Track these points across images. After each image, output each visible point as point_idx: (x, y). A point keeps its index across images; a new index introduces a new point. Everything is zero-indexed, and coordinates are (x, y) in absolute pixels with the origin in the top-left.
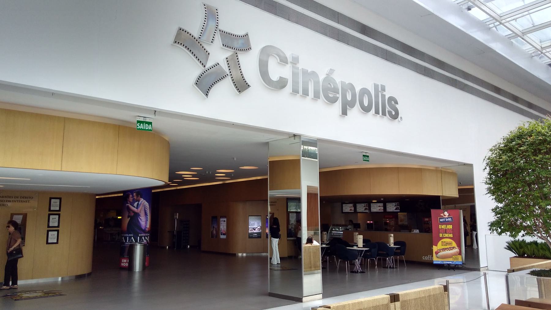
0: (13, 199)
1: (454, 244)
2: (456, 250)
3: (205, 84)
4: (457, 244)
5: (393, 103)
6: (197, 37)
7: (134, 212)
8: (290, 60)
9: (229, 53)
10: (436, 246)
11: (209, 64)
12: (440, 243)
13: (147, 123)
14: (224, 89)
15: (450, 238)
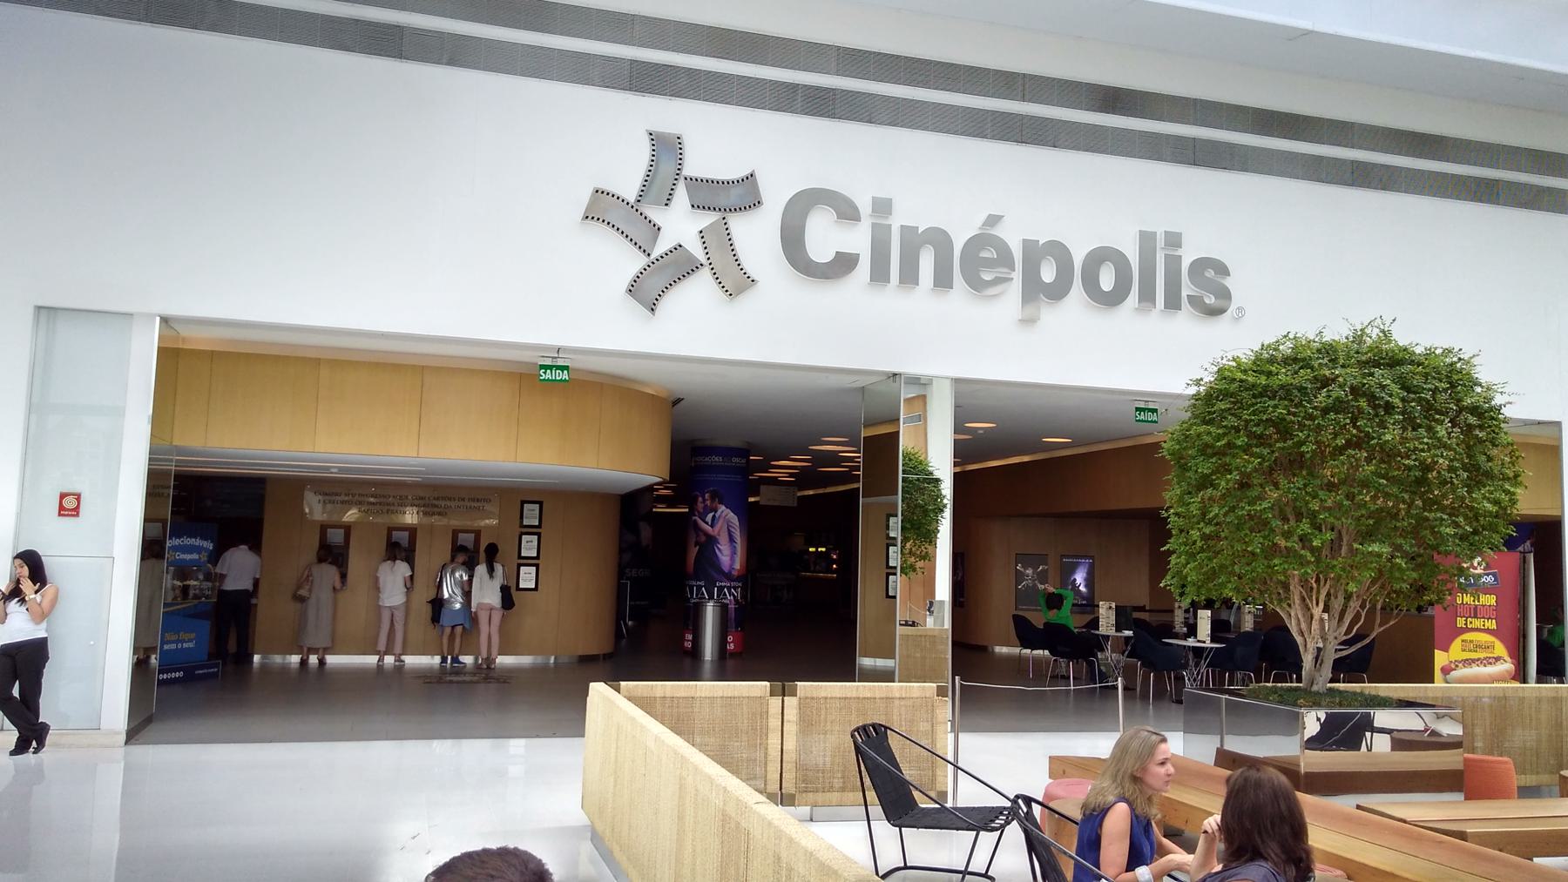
0: (457, 503)
1: (1500, 649)
2: (1507, 666)
3: (647, 291)
4: (1507, 648)
5: (1210, 273)
6: (632, 200)
7: (706, 534)
8: (865, 207)
9: (708, 219)
10: (1446, 649)
11: (661, 248)
12: (1456, 645)
13: (558, 367)
14: (698, 292)
15: (1488, 631)
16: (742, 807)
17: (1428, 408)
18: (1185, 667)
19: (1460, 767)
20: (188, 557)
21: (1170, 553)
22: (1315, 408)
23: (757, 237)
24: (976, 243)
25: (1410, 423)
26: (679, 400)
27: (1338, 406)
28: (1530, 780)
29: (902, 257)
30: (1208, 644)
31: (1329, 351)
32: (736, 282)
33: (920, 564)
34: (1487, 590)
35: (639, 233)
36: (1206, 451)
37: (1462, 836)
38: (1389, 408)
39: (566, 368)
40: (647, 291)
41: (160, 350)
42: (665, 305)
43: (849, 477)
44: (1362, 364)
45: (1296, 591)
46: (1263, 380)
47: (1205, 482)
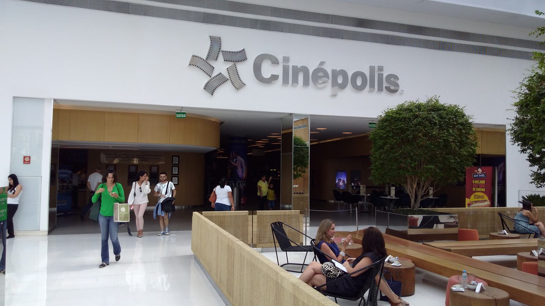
1: (486, 198)
2: (488, 203)
3: (210, 88)
4: (488, 197)
5: (392, 79)
6: (205, 58)
7: (234, 166)
8: (280, 59)
11: (215, 74)
12: (473, 196)
14: (226, 89)
16: (233, 242)
17: (448, 124)
18: (386, 205)
19: (457, 232)
20: (64, 176)
21: (372, 169)
22: (413, 124)
23: (245, 70)
24: (316, 71)
25: (441, 128)
26: (223, 123)
27: (420, 124)
28: (482, 236)
29: (294, 75)
30: (394, 198)
31: (419, 107)
32: (239, 85)
33: (303, 174)
34: (481, 179)
35: (208, 70)
36: (381, 138)
37: (450, 250)
38: (435, 124)
39: (185, 113)
40: (210, 88)
41: (54, 110)
42: (217, 93)
43: (279, 146)
44: (430, 110)
45: (409, 180)
46: (398, 116)
47: (381, 147)
